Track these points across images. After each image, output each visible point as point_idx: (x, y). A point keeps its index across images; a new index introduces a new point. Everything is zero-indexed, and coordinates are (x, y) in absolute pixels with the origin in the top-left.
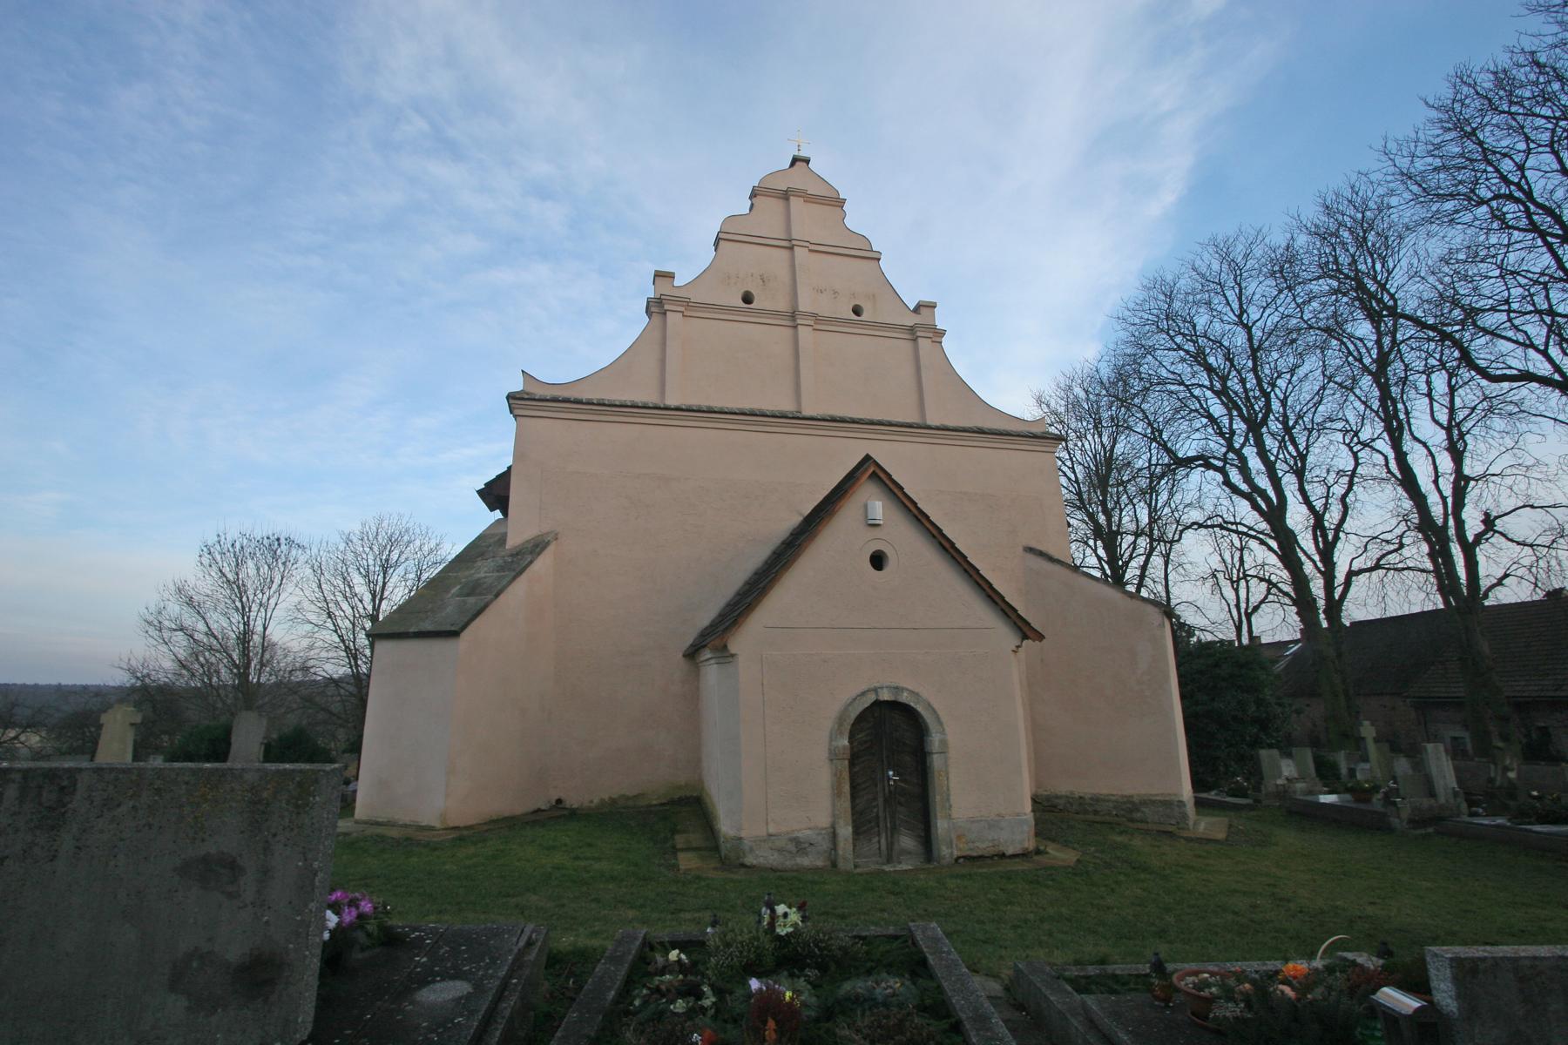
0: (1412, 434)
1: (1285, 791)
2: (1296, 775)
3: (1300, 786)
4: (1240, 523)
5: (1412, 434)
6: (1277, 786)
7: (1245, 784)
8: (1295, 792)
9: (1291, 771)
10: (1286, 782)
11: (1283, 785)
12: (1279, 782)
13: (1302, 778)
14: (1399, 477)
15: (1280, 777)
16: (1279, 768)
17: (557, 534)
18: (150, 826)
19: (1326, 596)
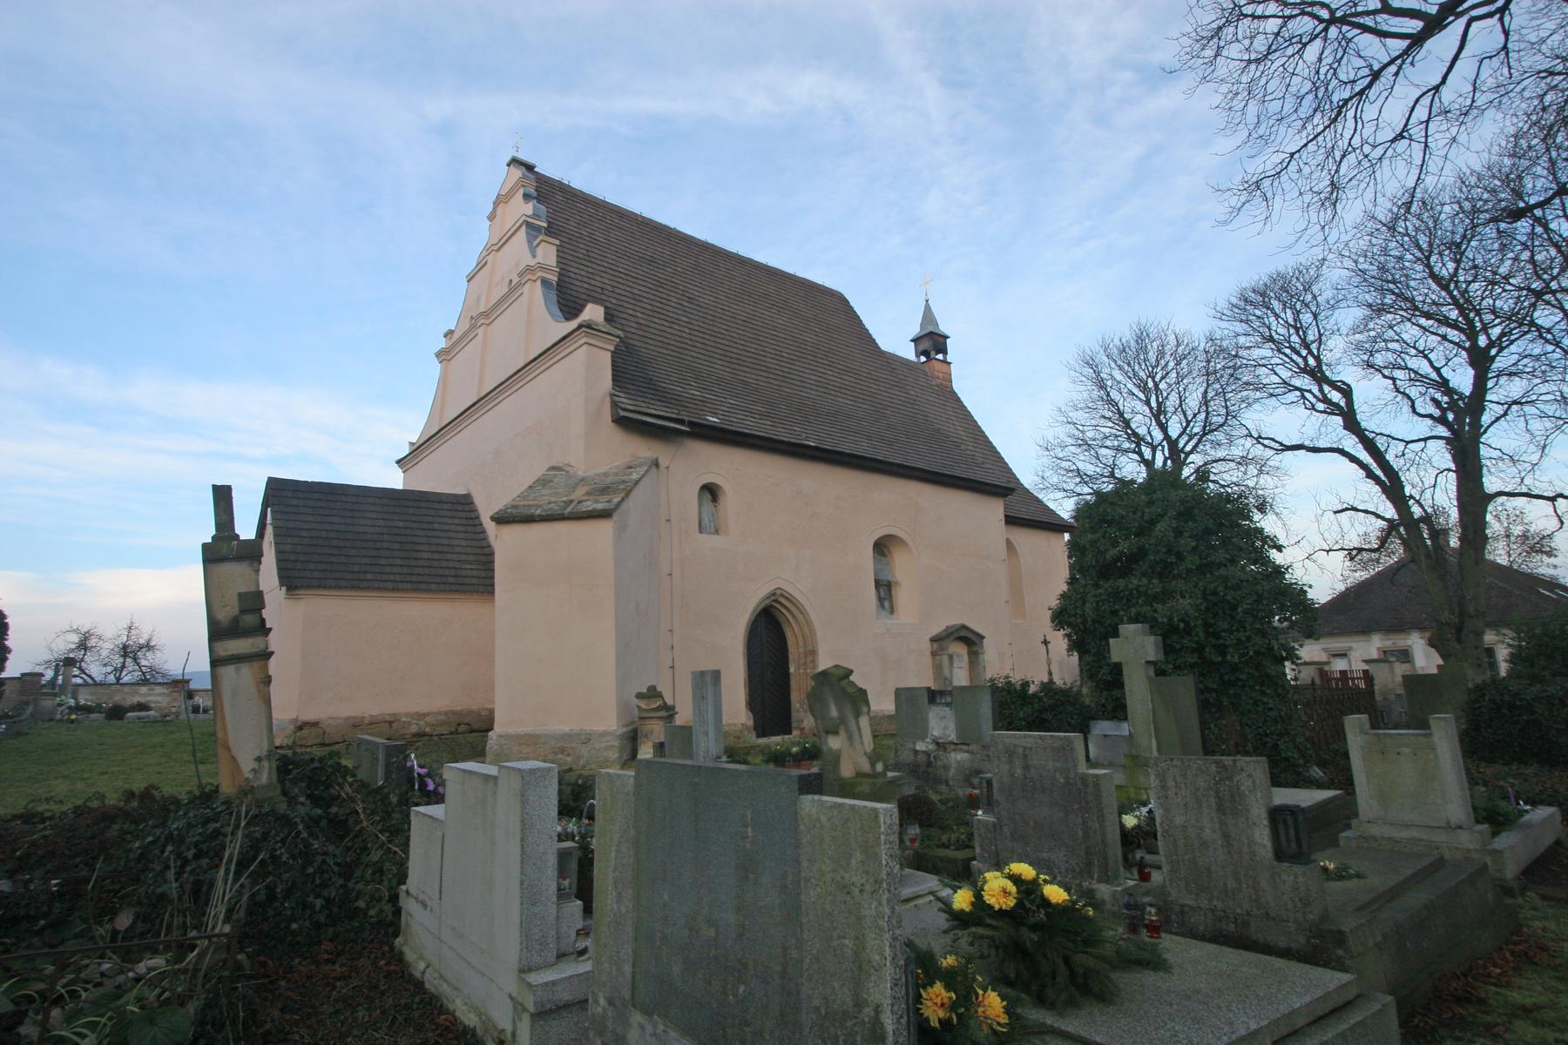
0: (1342, 452)
1: (929, 764)
2: (953, 737)
3: (958, 757)
4: (1345, 52)
5: (1342, 452)
6: (916, 752)
7: (1467, 428)
8: (946, 768)
9: (945, 728)
10: (932, 747)
11: (927, 754)
12: (920, 746)
13: (962, 743)
14: (1367, 433)
15: (923, 738)
16: (925, 721)
17: (878, 1006)
18: (1338, 330)
19: (1455, 459)
